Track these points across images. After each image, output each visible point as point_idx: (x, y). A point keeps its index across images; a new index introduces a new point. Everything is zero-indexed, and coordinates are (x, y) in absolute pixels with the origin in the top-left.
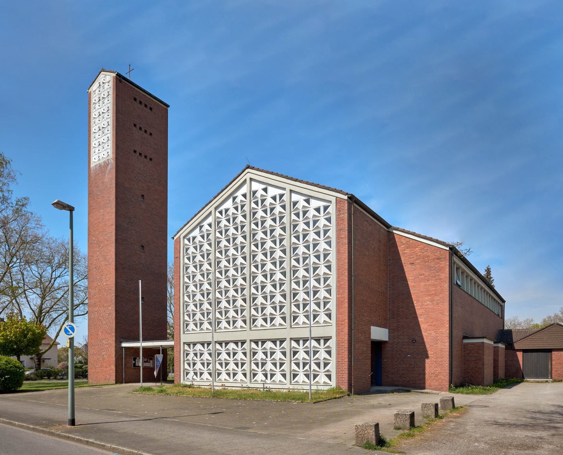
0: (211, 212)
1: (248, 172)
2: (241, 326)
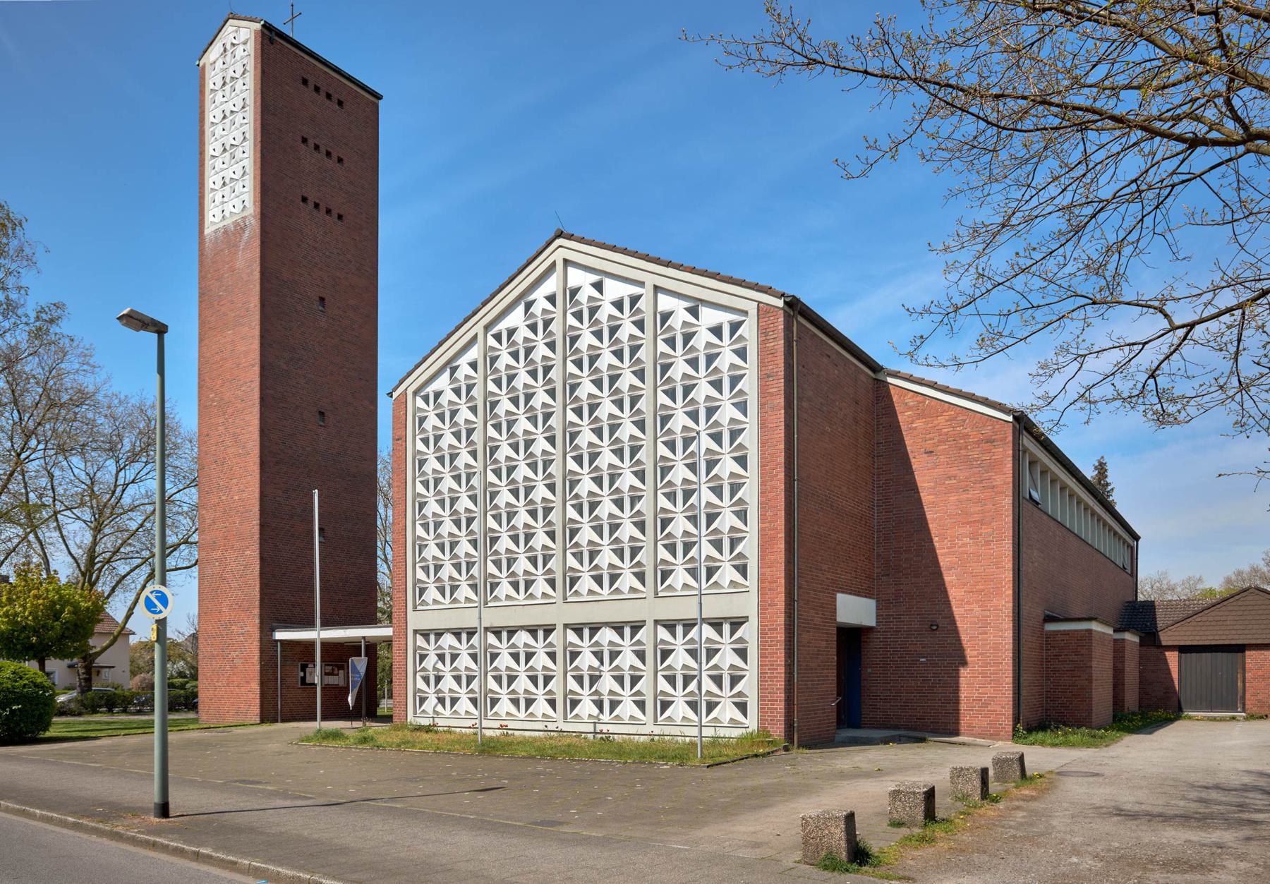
1: (560, 246)
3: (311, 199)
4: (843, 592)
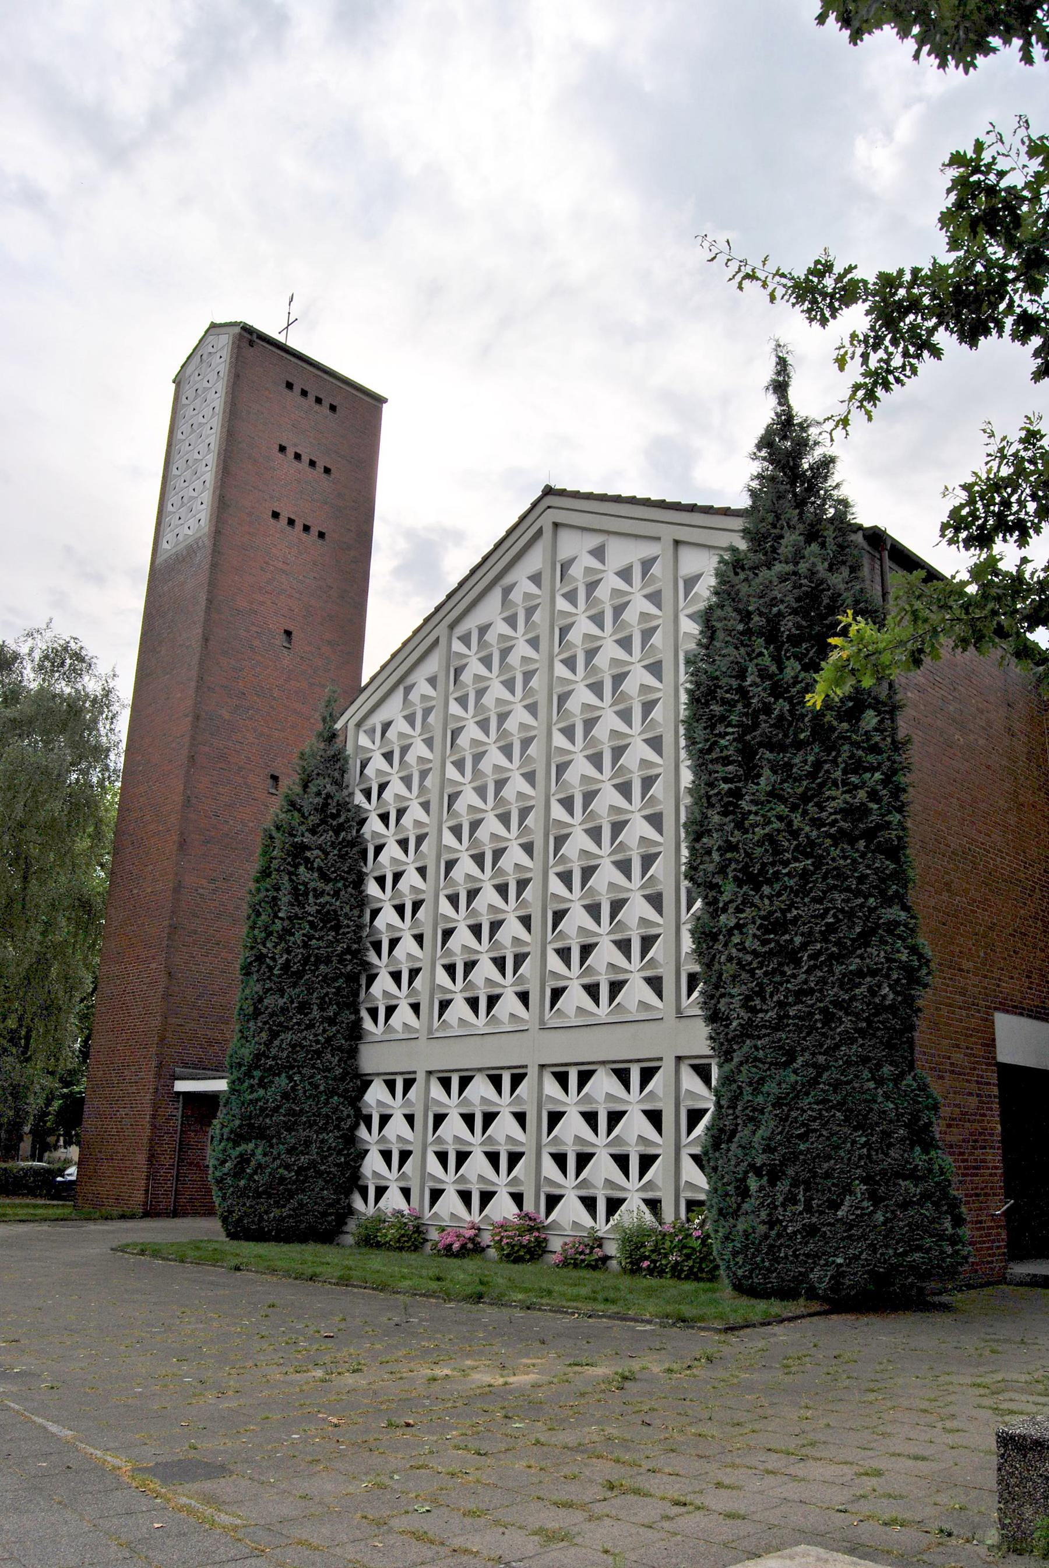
0: (437, 641)
1: (549, 507)
2: (512, 1015)
3: (284, 516)
4: (1007, 1012)
